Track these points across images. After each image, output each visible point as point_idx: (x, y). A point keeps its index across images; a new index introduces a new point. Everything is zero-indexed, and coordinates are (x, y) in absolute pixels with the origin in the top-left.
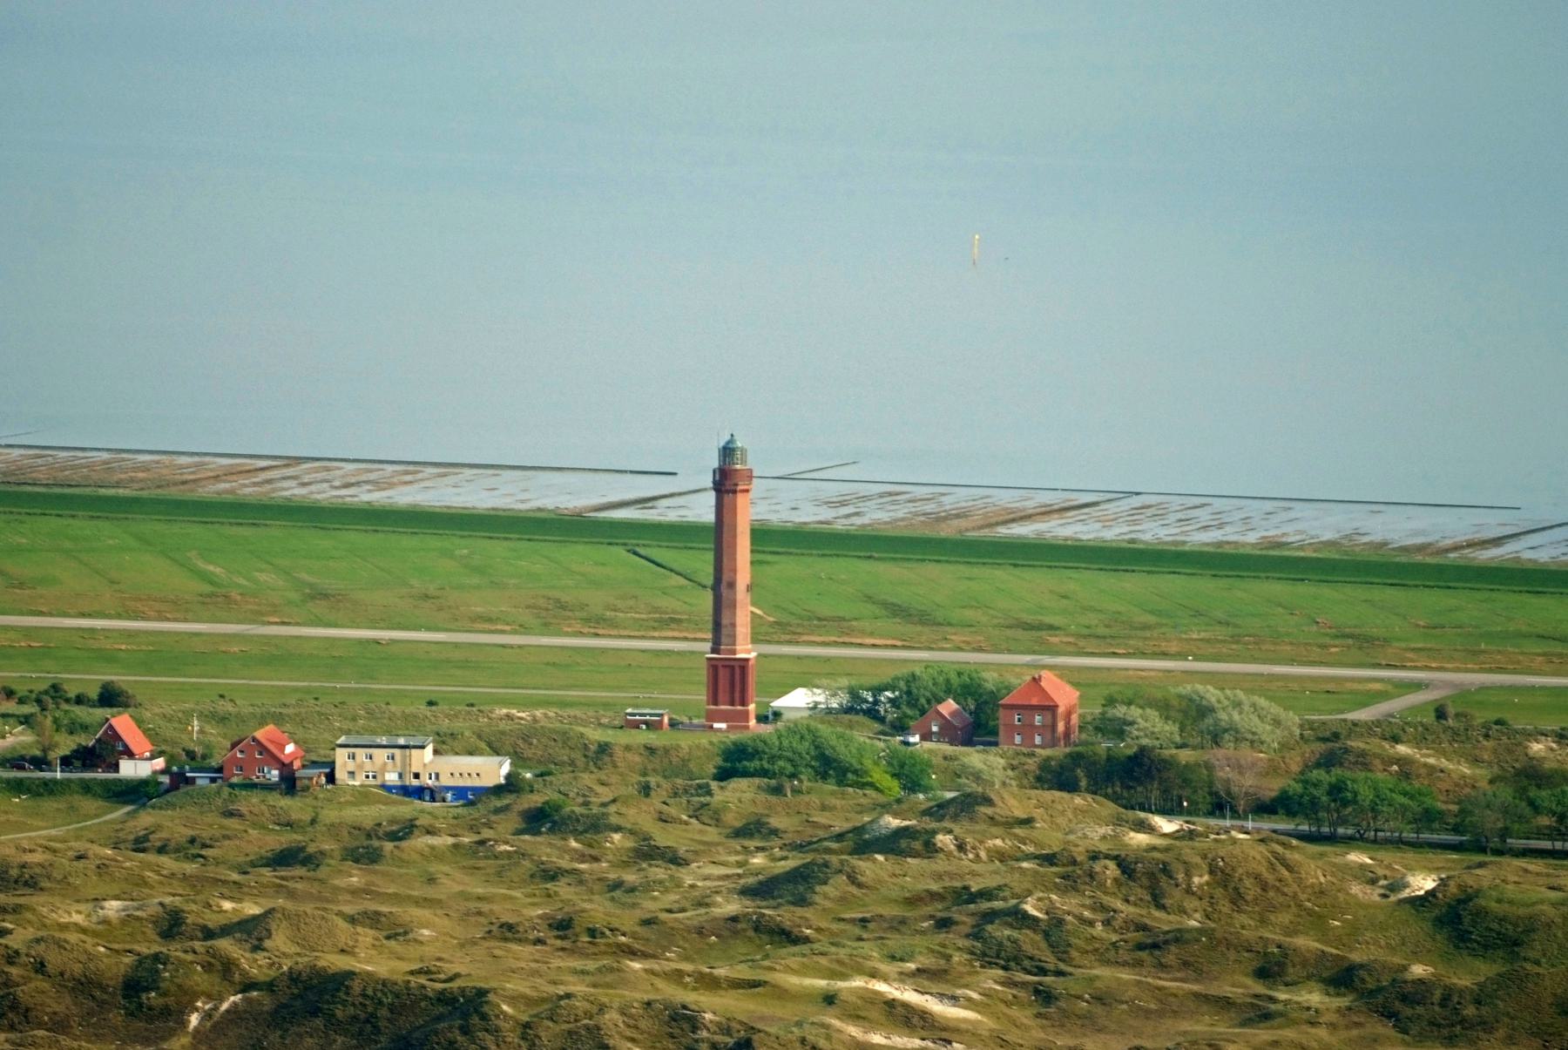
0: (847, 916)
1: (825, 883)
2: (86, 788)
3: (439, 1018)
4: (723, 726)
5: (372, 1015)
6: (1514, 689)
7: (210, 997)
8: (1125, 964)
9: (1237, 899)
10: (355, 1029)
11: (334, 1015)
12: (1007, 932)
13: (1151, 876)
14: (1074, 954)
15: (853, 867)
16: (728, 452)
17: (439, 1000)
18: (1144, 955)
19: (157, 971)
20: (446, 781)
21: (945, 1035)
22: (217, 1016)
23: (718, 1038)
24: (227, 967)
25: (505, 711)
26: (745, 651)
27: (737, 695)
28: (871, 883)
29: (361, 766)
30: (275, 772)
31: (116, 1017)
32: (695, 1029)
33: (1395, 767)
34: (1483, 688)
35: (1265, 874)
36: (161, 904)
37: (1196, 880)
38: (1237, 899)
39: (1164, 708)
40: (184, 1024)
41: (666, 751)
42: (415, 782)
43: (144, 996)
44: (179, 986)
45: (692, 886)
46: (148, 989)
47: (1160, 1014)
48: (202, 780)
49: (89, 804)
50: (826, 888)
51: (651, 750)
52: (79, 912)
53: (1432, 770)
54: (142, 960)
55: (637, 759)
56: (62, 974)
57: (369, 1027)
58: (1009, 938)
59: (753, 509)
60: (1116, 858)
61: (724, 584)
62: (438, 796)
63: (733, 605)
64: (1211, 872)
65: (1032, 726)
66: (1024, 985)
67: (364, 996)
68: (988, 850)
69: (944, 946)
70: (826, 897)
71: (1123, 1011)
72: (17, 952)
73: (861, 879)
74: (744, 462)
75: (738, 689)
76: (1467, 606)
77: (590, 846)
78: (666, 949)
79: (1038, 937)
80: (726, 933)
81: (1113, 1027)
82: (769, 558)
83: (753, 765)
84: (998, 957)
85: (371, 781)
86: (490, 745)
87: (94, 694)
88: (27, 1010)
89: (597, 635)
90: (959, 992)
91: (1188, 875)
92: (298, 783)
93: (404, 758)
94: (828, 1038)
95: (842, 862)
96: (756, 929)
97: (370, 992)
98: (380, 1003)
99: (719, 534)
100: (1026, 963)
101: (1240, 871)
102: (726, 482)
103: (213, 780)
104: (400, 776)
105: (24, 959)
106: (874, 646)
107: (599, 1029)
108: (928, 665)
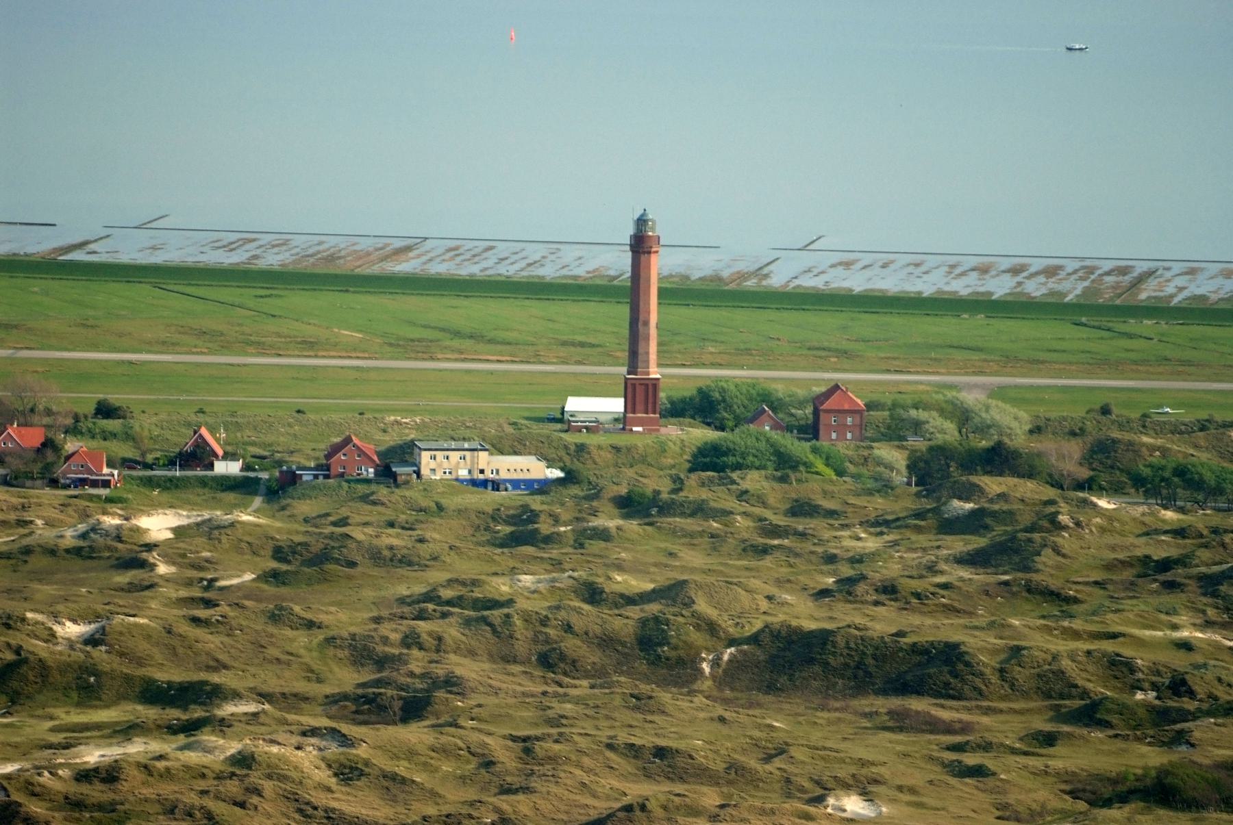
0: (1080, 580)
1: (1039, 554)
2: (203, 482)
4: (640, 429)
5: (859, 663)
6: (468, 371)
7: (708, 650)
10: (849, 673)
11: (828, 663)
16: (641, 222)
19: (663, 630)
20: (504, 475)
22: (724, 665)
23: (1154, 679)
25: (392, 418)
26: (655, 373)
29: (440, 465)
30: (371, 470)
31: (642, 666)
36: (570, 577)
39: (942, 412)
40: (701, 671)
41: (629, 449)
42: (481, 477)
44: (685, 642)
45: (901, 557)
46: (661, 644)
48: (307, 477)
51: (617, 449)
54: (644, 622)
55: (609, 456)
59: (661, 264)
62: (502, 487)
63: (647, 339)
67: (849, 648)
69: (1193, 603)
72: (546, 617)
74: (653, 229)
75: (650, 400)
83: (731, 460)
85: (448, 476)
87: (91, 408)
93: (473, 457)
95: (1043, 539)
96: (1029, 591)
97: (852, 645)
98: (864, 654)
102: (641, 244)
104: (470, 472)
107: (1063, 673)
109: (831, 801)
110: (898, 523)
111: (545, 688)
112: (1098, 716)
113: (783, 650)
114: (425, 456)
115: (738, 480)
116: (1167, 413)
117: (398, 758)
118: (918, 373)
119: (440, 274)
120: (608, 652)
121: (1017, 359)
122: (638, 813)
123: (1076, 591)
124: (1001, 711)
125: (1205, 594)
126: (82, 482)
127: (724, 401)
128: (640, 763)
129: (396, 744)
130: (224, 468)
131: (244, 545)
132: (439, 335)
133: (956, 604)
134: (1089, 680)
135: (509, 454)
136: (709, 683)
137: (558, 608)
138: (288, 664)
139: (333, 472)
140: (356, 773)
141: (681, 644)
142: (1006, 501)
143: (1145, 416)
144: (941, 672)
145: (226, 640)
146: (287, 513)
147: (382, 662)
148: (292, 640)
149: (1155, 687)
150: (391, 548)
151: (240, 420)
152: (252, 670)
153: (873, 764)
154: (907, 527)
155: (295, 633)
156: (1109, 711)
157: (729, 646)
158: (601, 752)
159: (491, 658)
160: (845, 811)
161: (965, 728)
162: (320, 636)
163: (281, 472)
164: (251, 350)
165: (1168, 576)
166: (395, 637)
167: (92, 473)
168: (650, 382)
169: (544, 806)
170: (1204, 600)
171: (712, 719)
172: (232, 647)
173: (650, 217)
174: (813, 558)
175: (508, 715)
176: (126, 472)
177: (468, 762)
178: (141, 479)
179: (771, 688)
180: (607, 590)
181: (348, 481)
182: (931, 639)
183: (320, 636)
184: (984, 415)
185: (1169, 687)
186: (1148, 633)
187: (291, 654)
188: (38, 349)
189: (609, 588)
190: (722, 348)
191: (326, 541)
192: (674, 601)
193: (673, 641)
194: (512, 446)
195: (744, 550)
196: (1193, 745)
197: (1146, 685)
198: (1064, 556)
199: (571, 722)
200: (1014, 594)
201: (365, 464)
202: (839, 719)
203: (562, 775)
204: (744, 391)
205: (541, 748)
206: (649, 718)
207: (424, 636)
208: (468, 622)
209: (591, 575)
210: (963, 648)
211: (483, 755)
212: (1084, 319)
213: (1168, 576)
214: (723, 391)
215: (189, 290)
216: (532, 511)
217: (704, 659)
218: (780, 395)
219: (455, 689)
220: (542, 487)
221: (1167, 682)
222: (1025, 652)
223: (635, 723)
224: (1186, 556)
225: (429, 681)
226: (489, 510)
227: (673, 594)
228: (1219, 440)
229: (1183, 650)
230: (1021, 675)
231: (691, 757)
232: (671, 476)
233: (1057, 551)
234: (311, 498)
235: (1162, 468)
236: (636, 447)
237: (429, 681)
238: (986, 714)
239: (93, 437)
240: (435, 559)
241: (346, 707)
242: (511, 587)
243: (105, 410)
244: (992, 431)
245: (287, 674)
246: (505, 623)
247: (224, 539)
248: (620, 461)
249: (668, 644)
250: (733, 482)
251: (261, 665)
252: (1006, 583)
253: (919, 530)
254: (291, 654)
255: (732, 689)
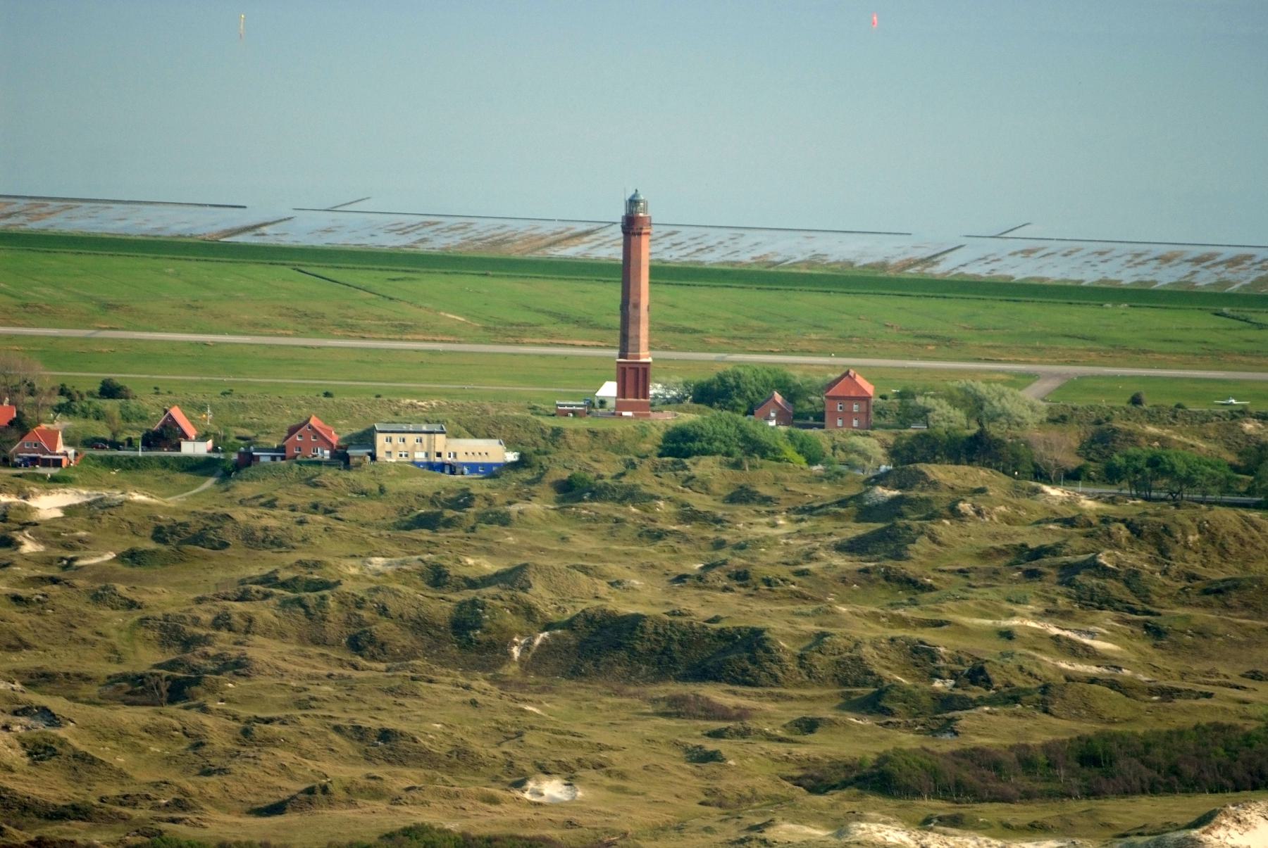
0: (946, 568)
1: (914, 542)
2: (164, 463)
3: (724, 651)
4: (629, 414)
7: (522, 634)
8: (1198, 605)
9: (1223, 551)
10: (654, 659)
11: (634, 649)
12: (1095, 581)
13: (1155, 534)
14: (1155, 598)
15: (931, 530)
16: (633, 202)
17: (719, 637)
18: (1211, 598)
19: (478, 614)
20: (462, 458)
21: (1115, 663)
22: (534, 650)
23: (954, 667)
25: (408, 401)
26: (646, 357)
27: (640, 391)
28: (946, 542)
29: (396, 447)
30: (327, 452)
31: (452, 650)
32: (934, 659)
33: (1157, 444)
34: (1082, 378)
35: (1242, 534)
36: (420, 560)
37: (1191, 538)
38: (1223, 551)
39: (951, 399)
40: (510, 655)
41: (606, 434)
42: (438, 460)
43: (471, 633)
44: (498, 625)
45: (787, 544)
46: (474, 628)
47: (1249, 644)
48: (265, 458)
50: (916, 546)
51: (594, 434)
52: (354, 566)
53: (1185, 446)
54: (461, 605)
55: (585, 440)
56: (401, 616)
57: (666, 658)
58: (1098, 585)
59: (649, 252)
60: (1123, 521)
61: (630, 307)
62: (458, 470)
63: (638, 321)
64: (1200, 532)
65: (851, 412)
66: (1135, 622)
67: (657, 633)
68: (998, 515)
69: (1046, 592)
70: (918, 553)
71: (1221, 643)
72: (362, 599)
73: (940, 539)
74: (645, 210)
76: (995, 312)
77: (646, 511)
78: (826, 595)
79: (1121, 585)
80: (864, 582)
81: (1217, 655)
82: (410, 275)
83: (697, 445)
84: (1092, 600)
85: (404, 459)
86: (468, 429)
87: (96, 388)
88: (383, 644)
89: (364, 338)
90: (1092, 628)
91: (1185, 534)
92: (352, 461)
93: (429, 440)
94: (1038, 666)
96: (887, 578)
97: (661, 630)
98: (671, 639)
99: (625, 271)
100: (1117, 604)
101: (1223, 531)
102: (632, 226)
103: (274, 458)
104: (427, 455)
105: (369, 605)
106: (584, 346)
107: (861, 660)
109: (531, 785)
110: (824, 510)
111: (341, 671)
112: (882, 704)
113: (595, 634)
114: (380, 439)
115: (691, 466)
116: (1231, 404)
117: (106, 739)
118: (1009, 362)
119: (579, 256)
120: (420, 635)
121: (1124, 349)
122: (319, 795)
123: (935, 579)
124: (791, 698)
125: (1060, 584)
126: (34, 461)
127: (738, 387)
128: (363, 746)
129: (108, 724)
130: (194, 448)
131: (124, 525)
132: (542, 318)
133: (806, 592)
134: (888, 668)
135: (483, 437)
136: (515, 668)
137: (376, 590)
138: (93, 644)
139: (288, 454)
140: (49, 753)
141: (494, 627)
142: (936, 489)
143: (1179, 406)
144: (740, 658)
145: (35, 618)
146: (228, 494)
147: (189, 643)
148: (106, 620)
149: (954, 675)
150: (266, 529)
151: (247, 401)
152: (54, 649)
153: (611, 749)
154: (827, 514)
155: (114, 613)
156: (893, 699)
157: (545, 629)
158: (324, 734)
159: (301, 640)
160: (542, 795)
161: (742, 714)
162: (137, 615)
163: (240, 453)
164: (339, 332)
165: (1033, 565)
166: (207, 618)
167: (45, 452)
168: (640, 367)
169: (236, 788)
170: (1059, 589)
171: (464, 702)
172: (40, 626)
173: (642, 197)
174: (703, 544)
175: (260, 697)
176: (88, 452)
177: (180, 742)
178: (101, 458)
179: (575, 673)
180: (452, 573)
181: (298, 463)
182: (737, 625)
183: (137, 615)
184: (995, 403)
185: (967, 676)
186: (978, 621)
187: (100, 634)
188: (123, 329)
189: (454, 570)
190: (827, 335)
191: (206, 522)
192: (512, 584)
193: (487, 625)
194: (487, 430)
195: (640, 535)
196: (956, 734)
197: (945, 673)
198: (939, 544)
199: (319, 704)
200: (871, 582)
201: (321, 446)
202: (621, 704)
203: (263, 756)
204: (760, 377)
205: (260, 729)
206: (400, 701)
207: (236, 617)
208: (284, 604)
209: (441, 558)
210: (767, 634)
211: (198, 736)
212: (1226, 310)
213: (1033, 565)
214: (738, 376)
215: (330, 273)
216: (470, 495)
217: (516, 644)
218: (798, 381)
219: (241, 671)
220: (492, 471)
221: (966, 670)
222: (827, 639)
223: (383, 706)
224: (1058, 545)
225: (221, 663)
226: (429, 493)
227: (511, 578)
228: (1229, 430)
229: (1004, 639)
230: (821, 662)
231: (414, 740)
232: (625, 461)
233: (933, 539)
234: (258, 479)
235: (1137, 458)
236: (614, 432)
237: (221, 663)
238: (776, 701)
239: (86, 417)
240: (304, 540)
241: (121, 688)
242: (361, 569)
243: (109, 391)
244: (1002, 420)
245: (90, 654)
246: (319, 605)
247: (105, 519)
248: (595, 446)
249: (481, 627)
250: (685, 468)
251: (65, 645)
252: (866, 571)
253: (837, 517)
254: (100, 634)
255: (537, 674)
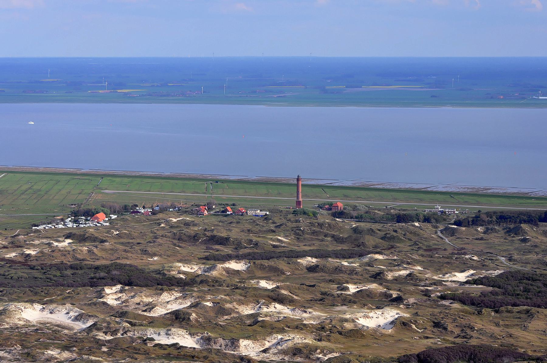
9: (331, 228)
16: (298, 176)
24: (205, 234)
26: (301, 199)
31: (192, 240)
49: (221, 217)
59: (300, 183)
99: (297, 185)
102: (298, 180)
108: (534, 211)
